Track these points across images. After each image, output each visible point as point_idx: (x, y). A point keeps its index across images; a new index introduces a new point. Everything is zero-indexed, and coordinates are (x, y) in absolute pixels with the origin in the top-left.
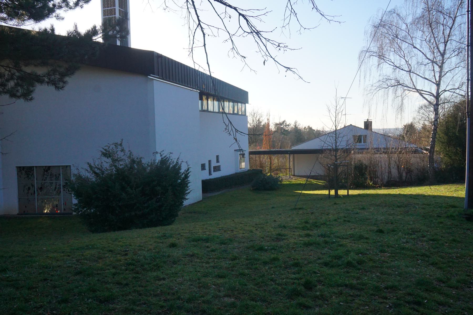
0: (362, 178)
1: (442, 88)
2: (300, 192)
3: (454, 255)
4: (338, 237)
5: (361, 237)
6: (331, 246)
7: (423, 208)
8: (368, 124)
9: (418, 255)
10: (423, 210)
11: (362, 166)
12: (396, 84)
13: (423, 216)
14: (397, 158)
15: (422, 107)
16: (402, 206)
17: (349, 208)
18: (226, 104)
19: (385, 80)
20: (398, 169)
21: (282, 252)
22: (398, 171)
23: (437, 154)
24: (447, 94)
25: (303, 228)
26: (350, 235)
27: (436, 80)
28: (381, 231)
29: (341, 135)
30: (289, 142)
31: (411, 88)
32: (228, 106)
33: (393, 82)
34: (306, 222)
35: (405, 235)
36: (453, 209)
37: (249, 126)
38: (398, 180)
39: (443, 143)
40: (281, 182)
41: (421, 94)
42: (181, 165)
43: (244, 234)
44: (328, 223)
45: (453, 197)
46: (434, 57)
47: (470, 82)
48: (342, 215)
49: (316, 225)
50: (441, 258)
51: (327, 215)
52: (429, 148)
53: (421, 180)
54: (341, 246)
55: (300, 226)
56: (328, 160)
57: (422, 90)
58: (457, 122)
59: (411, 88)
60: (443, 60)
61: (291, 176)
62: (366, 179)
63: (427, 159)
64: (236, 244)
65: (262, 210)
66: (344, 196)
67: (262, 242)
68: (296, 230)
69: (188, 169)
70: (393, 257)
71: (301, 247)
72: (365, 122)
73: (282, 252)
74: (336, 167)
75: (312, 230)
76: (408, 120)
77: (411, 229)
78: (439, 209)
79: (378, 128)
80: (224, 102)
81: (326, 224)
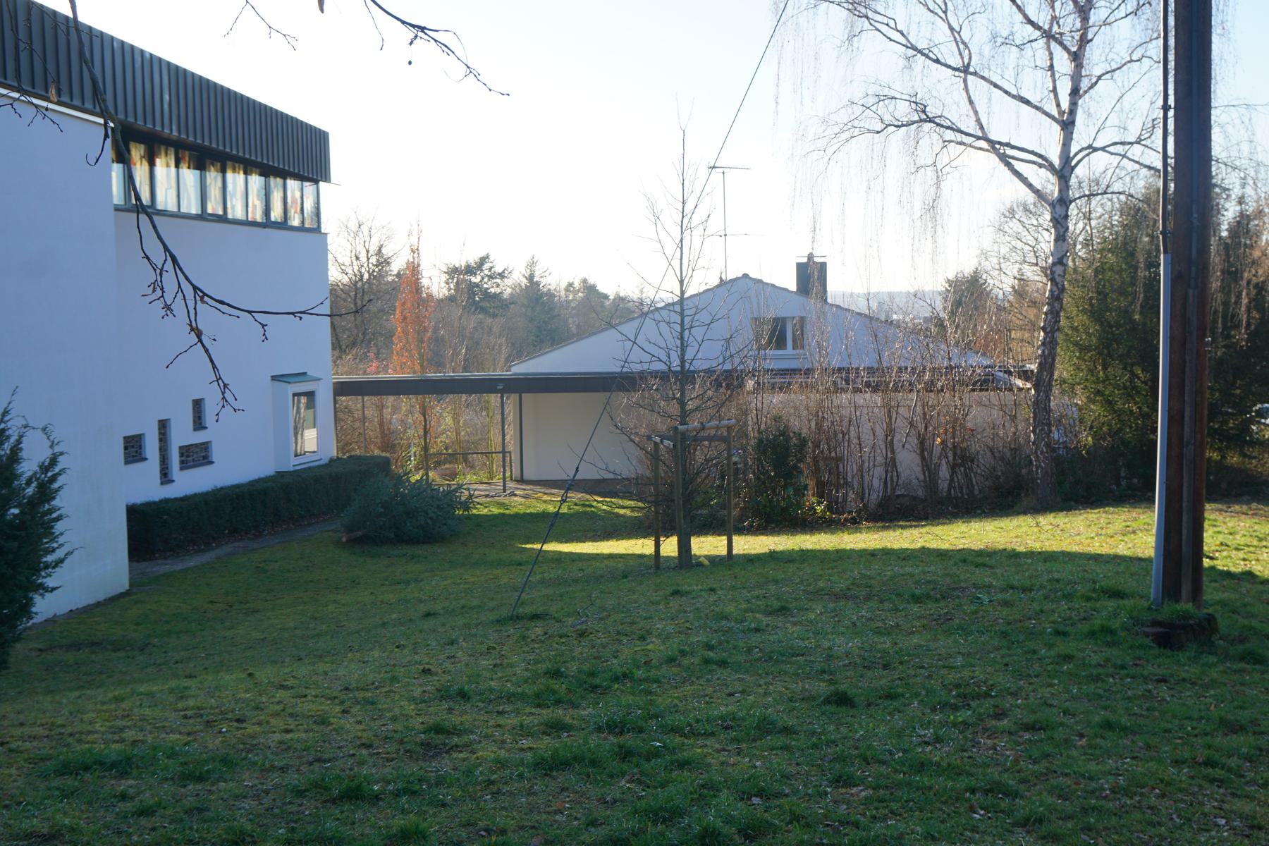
0: (785, 487)
1: (1081, 137)
2: (538, 546)
3: (1106, 784)
4: (675, 730)
5: (765, 727)
6: (647, 766)
7: (1006, 603)
8: (812, 276)
9: (973, 791)
10: (1005, 611)
11: (788, 439)
12: (916, 118)
13: (1004, 635)
14: (919, 410)
15: (1012, 212)
16: (928, 597)
17: (730, 609)
18: (236, 179)
19: (871, 100)
20: (923, 450)
21: (444, 805)
22: (923, 458)
23: (1063, 393)
24: (1099, 162)
25: (538, 696)
26: (722, 718)
27: (1058, 105)
28: (843, 700)
29: (704, 317)
30: (501, 340)
31: (967, 134)
32: (242, 193)
33: (903, 111)
34: (556, 674)
35: (934, 710)
36: (1111, 604)
37: (334, 275)
38: (920, 493)
39: (1083, 349)
40: (467, 509)
41: (1004, 159)
42: (19, 442)
43: (287, 731)
44: (639, 673)
45: (1116, 557)
46: (1054, 18)
47: (1171, 113)
48: (699, 637)
49: (592, 686)
50: (1060, 797)
51: (642, 638)
52: (1033, 367)
53: (1007, 493)
54: (682, 765)
55: (528, 689)
56: (648, 417)
57: (1008, 145)
58: (1136, 268)
59: (967, 134)
60: (1085, 29)
61: (511, 485)
62: (801, 491)
63: (1026, 413)
64: (249, 779)
65: (384, 625)
66: (714, 561)
67: (362, 763)
68: (507, 708)
69: (53, 461)
70: (881, 801)
71: (521, 776)
72: (799, 266)
73: (444, 805)
74: (684, 443)
75: (575, 706)
76: (964, 265)
77: (958, 686)
78: (1064, 605)
79: (848, 290)
80: (223, 171)
81: (632, 679)
